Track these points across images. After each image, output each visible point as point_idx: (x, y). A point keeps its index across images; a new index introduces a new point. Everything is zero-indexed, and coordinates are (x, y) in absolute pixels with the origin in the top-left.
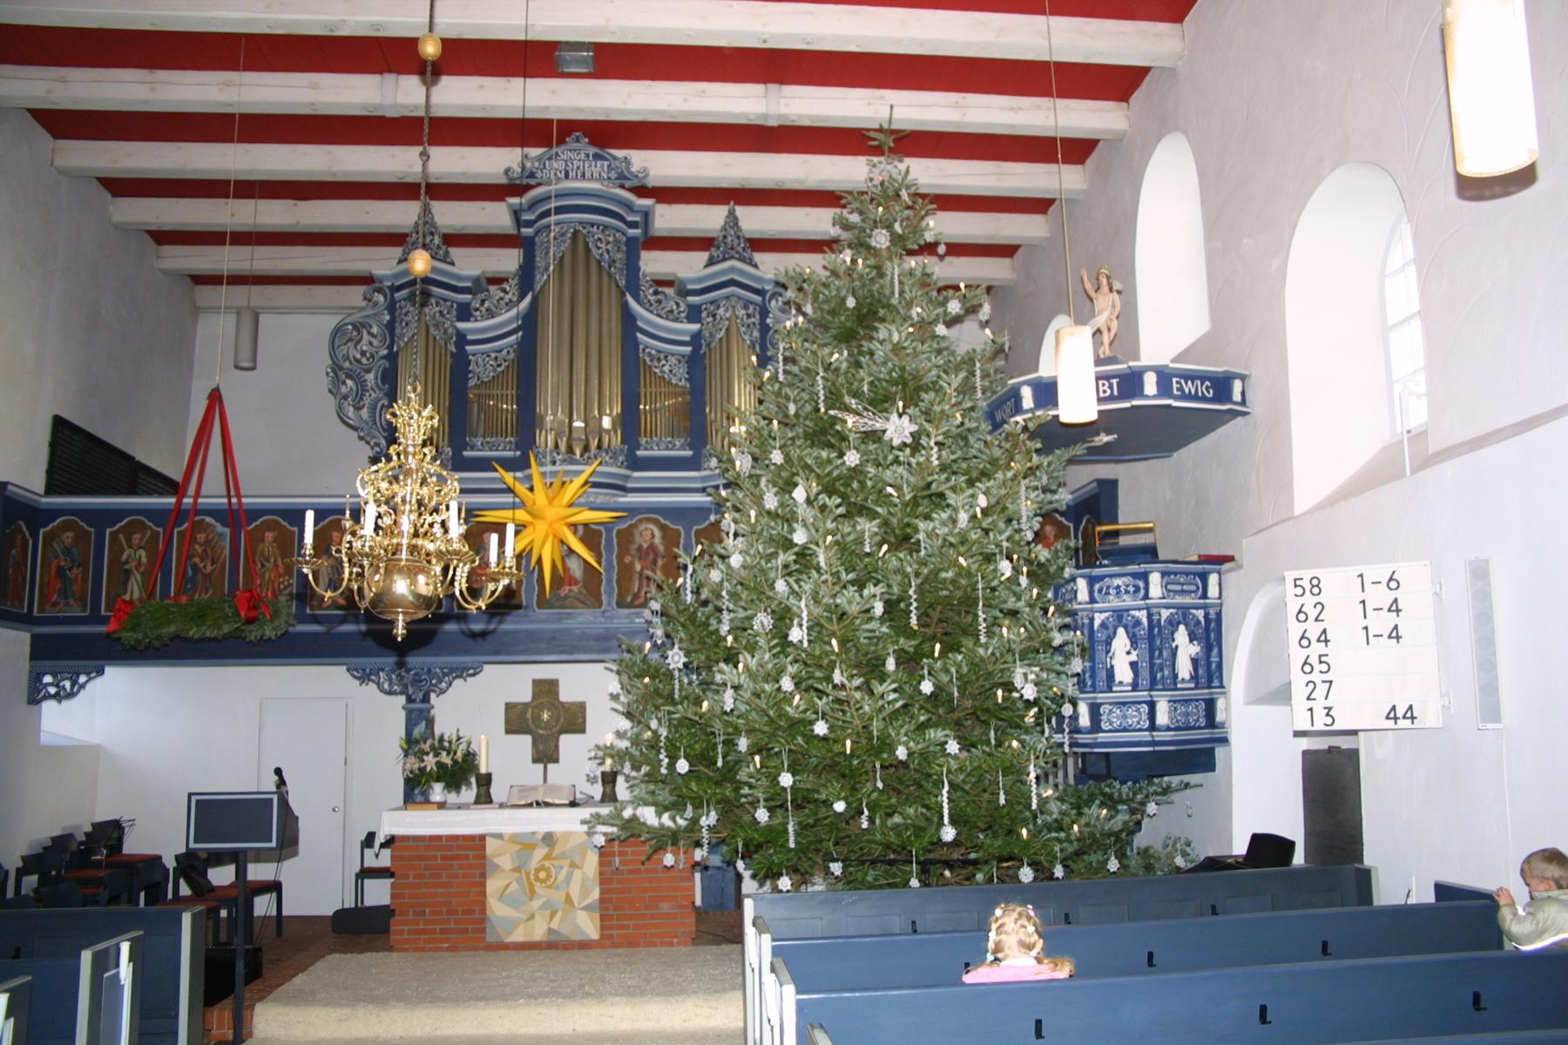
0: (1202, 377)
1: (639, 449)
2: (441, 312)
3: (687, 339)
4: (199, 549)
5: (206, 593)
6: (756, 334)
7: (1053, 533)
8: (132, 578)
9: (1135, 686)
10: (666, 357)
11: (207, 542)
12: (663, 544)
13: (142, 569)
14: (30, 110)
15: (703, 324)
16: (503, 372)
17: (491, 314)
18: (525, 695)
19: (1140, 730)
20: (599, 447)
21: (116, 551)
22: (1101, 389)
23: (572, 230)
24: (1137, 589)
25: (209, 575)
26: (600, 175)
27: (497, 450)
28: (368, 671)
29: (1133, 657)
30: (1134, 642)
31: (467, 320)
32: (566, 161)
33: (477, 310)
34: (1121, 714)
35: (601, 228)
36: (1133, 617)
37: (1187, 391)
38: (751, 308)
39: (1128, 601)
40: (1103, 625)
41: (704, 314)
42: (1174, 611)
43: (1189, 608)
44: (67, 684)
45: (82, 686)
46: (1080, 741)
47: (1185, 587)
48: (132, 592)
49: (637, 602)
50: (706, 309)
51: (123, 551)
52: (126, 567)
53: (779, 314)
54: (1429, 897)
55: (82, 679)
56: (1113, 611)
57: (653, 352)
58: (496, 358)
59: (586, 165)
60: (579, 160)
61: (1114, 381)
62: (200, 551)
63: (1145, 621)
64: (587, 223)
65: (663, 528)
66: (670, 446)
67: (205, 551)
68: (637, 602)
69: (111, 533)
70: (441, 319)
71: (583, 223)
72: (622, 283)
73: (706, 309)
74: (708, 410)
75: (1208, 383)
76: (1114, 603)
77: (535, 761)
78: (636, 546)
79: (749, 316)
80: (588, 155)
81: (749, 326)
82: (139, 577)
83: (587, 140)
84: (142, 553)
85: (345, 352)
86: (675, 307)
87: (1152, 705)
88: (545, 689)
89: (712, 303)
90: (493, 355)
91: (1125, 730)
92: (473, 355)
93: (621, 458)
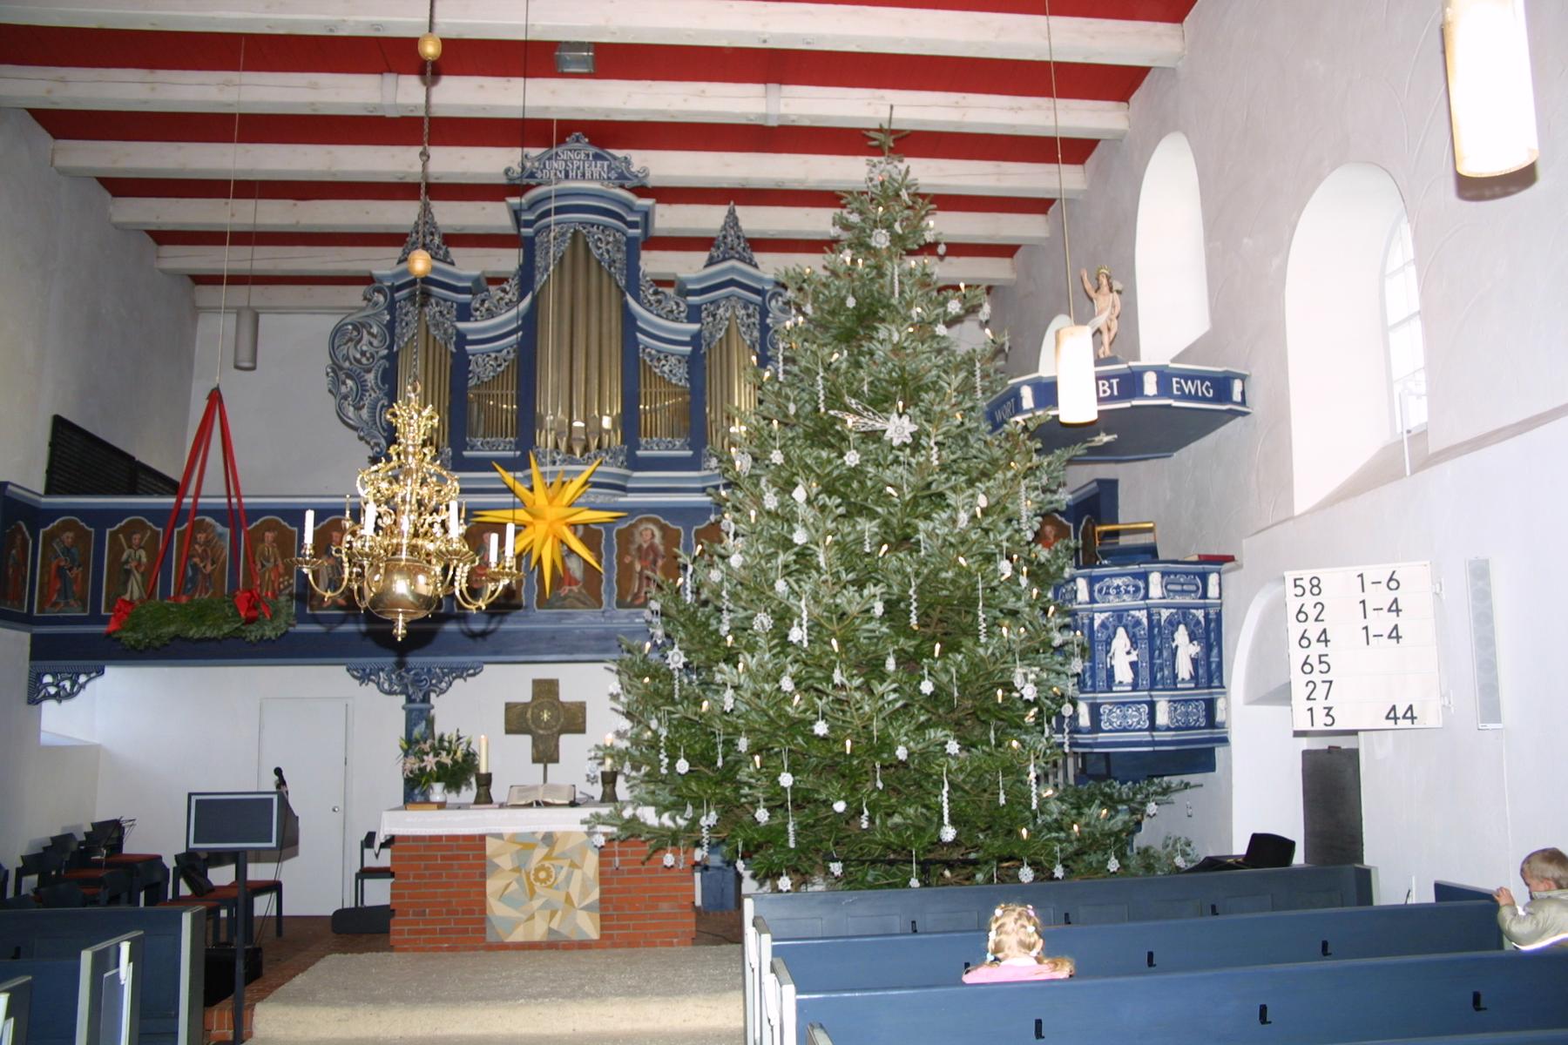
0: (1202, 377)
1: (639, 449)
2: (441, 312)
3: (687, 339)
4: (199, 549)
5: (206, 593)
6: (756, 334)
7: (1053, 533)
8: (132, 578)
9: (1135, 686)
10: (666, 357)
11: (207, 542)
12: (663, 544)
13: (142, 569)
14: (30, 110)
15: (703, 324)
16: (503, 372)
17: (491, 314)
18: (525, 695)
19: (1140, 730)
20: (599, 447)
21: (116, 551)
22: (1101, 389)
23: (572, 230)
24: (1137, 589)
25: (209, 575)
26: (600, 175)
27: (497, 450)
28: (368, 671)
29: (1133, 657)
30: (1134, 642)
31: (467, 320)
32: (566, 161)
33: (477, 310)
34: (1121, 714)
35: (601, 228)
36: (1133, 617)
37: (1187, 391)
38: (751, 308)
39: (1128, 601)
40: (1103, 625)
41: (704, 314)
42: (1174, 611)
43: (1189, 608)
44: (67, 684)
45: (82, 686)
46: (1080, 741)
47: (1185, 587)
48: (132, 592)
49: (637, 602)
50: (706, 309)
51: (123, 551)
52: (126, 567)
53: (779, 314)
54: (1429, 897)
55: (82, 679)
56: (1113, 611)
57: (653, 352)
58: (496, 358)
59: (586, 165)
60: (579, 160)
61: (1114, 381)
62: (200, 551)
63: (1145, 621)
64: (587, 223)
65: (663, 528)
66: (670, 446)
67: (205, 551)
68: (637, 602)
69: (111, 533)
70: (441, 319)
71: (583, 223)
72: (622, 283)
73: (706, 309)
74: (708, 410)
75: (1208, 383)
76: (1114, 603)
77: (535, 761)
78: (636, 546)
79: (749, 316)
80: (588, 155)
81: (749, 326)
82: (139, 577)
83: (587, 140)
84: (142, 553)
85: (345, 352)
86: (675, 307)
87: (1152, 705)
88: (545, 689)
89: (712, 303)
90: (493, 355)
91: (1125, 730)
92: (473, 355)
93: (621, 458)
